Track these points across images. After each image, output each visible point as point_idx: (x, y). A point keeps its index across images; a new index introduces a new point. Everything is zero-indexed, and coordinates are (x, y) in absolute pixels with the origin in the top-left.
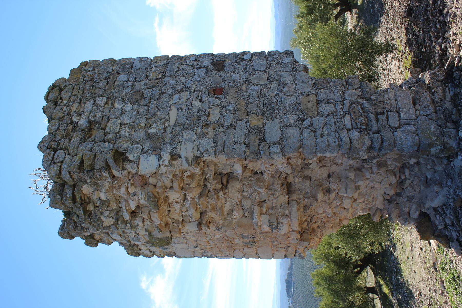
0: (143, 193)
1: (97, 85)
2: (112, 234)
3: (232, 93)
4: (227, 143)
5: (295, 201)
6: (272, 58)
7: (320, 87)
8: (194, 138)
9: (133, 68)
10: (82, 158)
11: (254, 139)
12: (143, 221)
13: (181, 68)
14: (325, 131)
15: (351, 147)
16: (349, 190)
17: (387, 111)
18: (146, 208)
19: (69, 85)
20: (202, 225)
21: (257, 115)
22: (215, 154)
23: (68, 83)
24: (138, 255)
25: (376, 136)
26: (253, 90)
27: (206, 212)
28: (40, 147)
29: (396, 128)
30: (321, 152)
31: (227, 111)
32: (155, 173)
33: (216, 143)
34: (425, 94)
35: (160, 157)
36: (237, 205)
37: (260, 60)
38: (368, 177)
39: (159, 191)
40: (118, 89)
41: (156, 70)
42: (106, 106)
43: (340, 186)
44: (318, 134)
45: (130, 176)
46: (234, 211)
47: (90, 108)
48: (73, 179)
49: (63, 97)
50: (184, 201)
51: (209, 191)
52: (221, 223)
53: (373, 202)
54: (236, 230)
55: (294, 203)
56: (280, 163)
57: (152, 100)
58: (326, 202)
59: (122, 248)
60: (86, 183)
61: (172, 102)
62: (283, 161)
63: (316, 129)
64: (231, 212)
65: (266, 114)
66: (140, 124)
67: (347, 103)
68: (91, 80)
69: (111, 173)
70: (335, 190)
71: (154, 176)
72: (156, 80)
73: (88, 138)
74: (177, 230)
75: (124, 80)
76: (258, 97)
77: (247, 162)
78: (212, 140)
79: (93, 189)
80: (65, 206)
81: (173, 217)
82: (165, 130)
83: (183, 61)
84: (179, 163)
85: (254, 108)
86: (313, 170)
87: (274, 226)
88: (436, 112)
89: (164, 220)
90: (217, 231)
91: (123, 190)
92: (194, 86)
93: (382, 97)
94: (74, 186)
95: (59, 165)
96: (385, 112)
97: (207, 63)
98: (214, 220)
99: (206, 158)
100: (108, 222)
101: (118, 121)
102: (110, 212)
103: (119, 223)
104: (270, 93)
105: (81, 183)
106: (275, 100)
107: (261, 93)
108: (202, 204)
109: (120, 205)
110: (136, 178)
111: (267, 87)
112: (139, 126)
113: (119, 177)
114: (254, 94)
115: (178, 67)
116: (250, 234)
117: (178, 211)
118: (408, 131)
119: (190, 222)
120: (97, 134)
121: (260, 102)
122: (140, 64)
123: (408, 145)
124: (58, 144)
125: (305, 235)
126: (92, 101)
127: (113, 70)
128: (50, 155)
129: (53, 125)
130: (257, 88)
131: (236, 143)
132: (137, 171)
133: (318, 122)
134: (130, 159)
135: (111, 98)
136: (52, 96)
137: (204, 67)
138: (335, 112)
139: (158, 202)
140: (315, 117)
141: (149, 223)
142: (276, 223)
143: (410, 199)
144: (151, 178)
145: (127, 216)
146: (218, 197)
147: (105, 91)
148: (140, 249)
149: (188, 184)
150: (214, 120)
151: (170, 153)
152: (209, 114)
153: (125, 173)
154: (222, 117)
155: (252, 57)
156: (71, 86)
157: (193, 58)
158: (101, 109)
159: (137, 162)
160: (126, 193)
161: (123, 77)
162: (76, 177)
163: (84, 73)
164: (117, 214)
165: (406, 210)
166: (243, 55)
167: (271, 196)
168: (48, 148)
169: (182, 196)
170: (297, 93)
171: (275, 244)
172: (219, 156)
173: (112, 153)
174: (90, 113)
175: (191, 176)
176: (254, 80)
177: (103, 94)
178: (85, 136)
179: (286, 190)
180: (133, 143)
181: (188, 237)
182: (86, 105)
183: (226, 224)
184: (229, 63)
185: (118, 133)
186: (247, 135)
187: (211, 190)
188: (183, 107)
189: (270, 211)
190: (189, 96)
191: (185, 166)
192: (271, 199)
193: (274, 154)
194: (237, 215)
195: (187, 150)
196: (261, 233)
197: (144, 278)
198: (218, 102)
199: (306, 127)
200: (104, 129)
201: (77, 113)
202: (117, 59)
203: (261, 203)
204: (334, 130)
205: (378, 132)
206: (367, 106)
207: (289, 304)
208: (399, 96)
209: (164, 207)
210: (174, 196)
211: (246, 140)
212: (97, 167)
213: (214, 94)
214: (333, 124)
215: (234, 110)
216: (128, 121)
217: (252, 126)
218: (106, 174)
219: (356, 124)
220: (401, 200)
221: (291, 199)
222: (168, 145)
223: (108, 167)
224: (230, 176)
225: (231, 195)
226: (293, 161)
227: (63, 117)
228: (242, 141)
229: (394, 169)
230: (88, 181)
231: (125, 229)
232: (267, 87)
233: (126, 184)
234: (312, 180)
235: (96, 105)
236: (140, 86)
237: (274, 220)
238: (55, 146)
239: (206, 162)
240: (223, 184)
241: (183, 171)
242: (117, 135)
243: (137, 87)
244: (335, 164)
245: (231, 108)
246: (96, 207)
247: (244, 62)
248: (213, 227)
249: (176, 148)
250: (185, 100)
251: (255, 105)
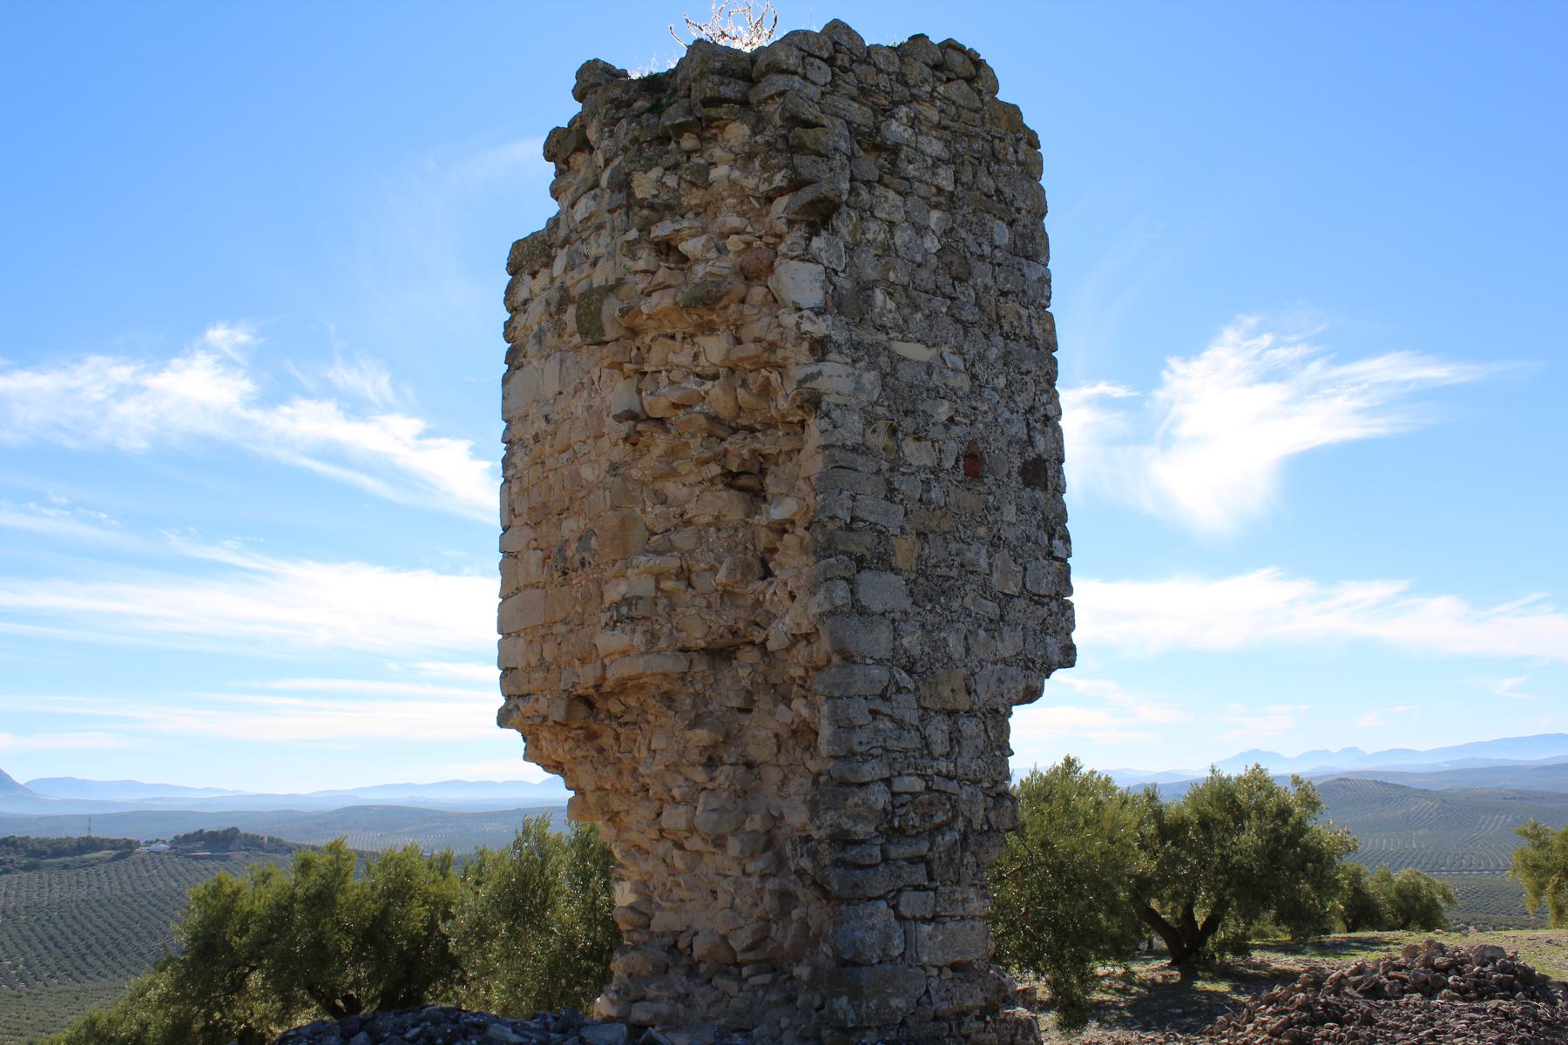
0: (726, 271)
2: (594, 197)
3: (970, 500)
4: (853, 475)
5: (690, 667)
7: (990, 723)
8: (864, 398)
10: (817, 125)
11: (863, 543)
12: (645, 272)
13: (1027, 378)
15: (849, 784)
16: (715, 816)
17: (935, 890)
20: (631, 423)
21: (920, 556)
22: (825, 447)
23: (987, 99)
24: (514, 268)
25: (877, 851)
26: (977, 553)
27: (668, 431)
28: (836, 27)
29: (895, 907)
30: (833, 712)
31: (926, 482)
32: (776, 301)
34: (981, 995)
35: (819, 312)
39: (730, 311)
40: (974, 219)
41: (1020, 317)
42: (934, 190)
43: (725, 795)
44: (878, 704)
45: (772, 240)
46: (663, 508)
47: (929, 151)
48: (765, 101)
49: (954, 86)
50: (698, 375)
51: (723, 440)
52: (634, 472)
55: (681, 665)
59: (540, 225)
60: (754, 133)
62: (805, 622)
65: (921, 580)
66: (894, 269)
67: (952, 787)
68: (993, 155)
69: (781, 191)
73: (859, 142)
74: (619, 359)
78: (859, 439)
79: (737, 149)
80: (695, 80)
81: (656, 348)
82: (882, 328)
83: (1045, 385)
84: (803, 359)
85: (934, 551)
86: (771, 714)
88: (936, 1018)
89: (652, 323)
90: (605, 466)
91: (735, 221)
93: (969, 880)
94: (745, 103)
95: (800, 70)
96: (933, 885)
97: (1041, 443)
98: (642, 456)
99: (815, 426)
100: (645, 185)
101: (898, 217)
102: (675, 190)
104: (971, 595)
105: (753, 120)
106: (955, 605)
109: (690, 215)
111: (985, 590)
112: (888, 268)
113: (768, 213)
114: (969, 556)
115: (1028, 372)
116: (595, 553)
117: (672, 358)
118: (889, 938)
119: (639, 391)
120: (869, 166)
121: (950, 567)
124: (845, 70)
125: (582, 710)
126: (945, 155)
127: (1018, 210)
128: (821, 48)
131: (854, 499)
132: (785, 255)
133: (907, 709)
134: (815, 239)
136: (957, 58)
138: (930, 753)
139: (705, 305)
141: (641, 286)
142: (634, 613)
143: (685, 998)
144: (763, 290)
145: (662, 230)
146: (706, 462)
147: (970, 189)
148: (534, 275)
149: (744, 384)
150: (907, 451)
151: (828, 337)
152: (918, 439)
153: (781, 226)
154: (913, 469)
155: (1057, 559)
158: (927, 177)
159: (807, 257)
160: (725, 230)
161: (1003, 235)
163: (1009, 138)
165: (652, 991)
166: (1061, 538)
167: (704, 603)
168: (835, 44)
169: (712, 371)
170: (973, 663)
171: (561, 629)
172: (820, 458)
173: (832, 195)
174: (916, 149)
175: (766, 391)
178: (862, 134)
179: (720, 643)
180: (850, 249)
181: (585, 394)
182: (934, 142)
187: (725, 445)
188: (935, 376)
189: (663, 602)
190: (960, 393)
192: (697, 601)
194: (653, 514)
195: (835, 377)
196: (599, 584)
197: (242, 338)
198: (948, 464)
200: (880, 181)
201: (916, 117)
203: (684, 575)
204: (888, 745)
205: (886, 859)
206: (947, 838)
207: (149, 843)
208: (973, 928)
209: (684, 324)
210: (715, 349)
212: (797, 159)
215: (930, 502)
216: (898, 242)
217: (894, 540)
218: (779, 179)
219: (903, 805)
221: (695, 656)
222: (846, 334)
223: (796, 185)
224: (757, 496)
225: (708, 496)
226: (802, 651)
229: (773, 940)
230: (758, 138)
232: (985, 590)
233: (749, 229)
234: (740, 716)
236: (982, 275)
237: (641, 610)
238: (839, 62)
239: (799, 429)
240: (739, 474)
243: (980, 268)
244: (785, 776)
245: (935, 494)
246: (689, 154)
248: (620, 452)
249: (840, 353)
251: (943, 554)
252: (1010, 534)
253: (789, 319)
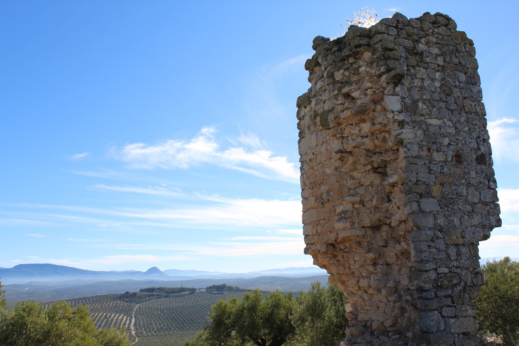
1: (454, 56)
2: (322, 81)
3: (458, 171)
4: (416, 166)
6: (493, 207)
7: (471, 248)
8: (418, 139)
9: (471, 86)
11: (421, 189)
12: (341, 104)
13: (476, 127)
14: (433, 250)
15: (422, 271)
16: (377, 282)
17: (455, 307)
18: (353, 105)
19: (451, 32)
21: (442, 192)
22: (406, 157)
24: (299, 105)
25: (433, 294)
26: (462, 189)
27: (353, 156)
29: (441, 313)
31: (442, 166)
32: (385, 110)
33: (416, 157)
35: (400, 112)
36: (359, 183)
37: (490, 196)
38: (390, 299)
39: (370, 115)
40: (452, 74)
41: (471, 106)
42: (436, 65)
43: (380, 275)
44: (430, 243)
45: (382, 90)
47: (433, 52)
48: (375, 44)
49: (440, 29)
50: (361, 136)
51: (371, 157)
52: (343, 170)
54: (336, 184)
55: (363, 232)
56: (398, 216)
57: (445, 103)
58: (365, 261)
60: (373, 55)
61: (445, 120)
62: (403, 217)
63: (434, 241)
64: (353, 178)
65: (443, 200)
66: (425, 94)
67: (459, 271)
68: (457, 50)
69: (383, 73)
70: (375, 270)
71: (383, 109)
72: (463, 106)
73: (409, 53)
75: (460, 79)
77: (400, 186)
78: (417, 154)
79: (368, 61)
82: (422, 115)
83: (483, 129)
85: (447, 189)
86: (394, 247)
90: (333, 168)
91: (369, 85)
92: (461, 138)
94: (369, 45)
95: (386, 32)
97: (483, 149)
98: (345, 164)
99: (402, 150)
101: (425, 76)
103: (339, 85)
104: (461, 204)
105: (372, 50)
106: (456, 208)
107: (461, 196)
109: (354, 84)
110: (381, 95)
111: (466, 201)
112: (423, 94)
113: (380, 81)
114: (459, 190)
115: (476, 124)
116: (332, 197)
117: (353, 132)
118: (439, 323)
119: (342, 143)
120: (413, 60)
121: (453, 195)
122: (476, 91)
123: (428, 322)
124: (401, 29)
125: (331, 248)
126: (439, 53)
127: (468, 68)
129: (416, 23)
130: (465, 192)
131: (417, 174)
132: (387, 94)
135: (443, 68)
136: (440, 19)
137: (478, 147)
138: (450, 259)
139: (362, 113)
140: (444, 241)
141: (340, 109)
142: (346, 216)
144: (380, 107)
145: (345, 90)
146: (366, 165)
147: (449, 63)
148: (305, 107)
149: (377, 138)
150: (434, 156)
151: (404, 120)
152: (438, 152)
153: (385, 85)
154: (437, 162)
155: (492, 189)
156: (450, 34)
158: (434, 61)
159: (394, 94)
160: (366, 88)
161: (463, 77)
162: (377, 46)
163: (462, 43)
164: (347, 82)
165: (359, 340)
166: (493, 181)
167: (369, 211)
168: (397, 21)
171: (322, 222)
172: (404, 161)
173: (401, 73)
174: (429, 52)
175: (384, 140)
176: (471, 190)
177: (447, 62)
178: (410, 50)
180: (409, 90)
181: (325, 145)
182: (435, 49)
183: (342, 174)
184: (485, 169)
187: (372, 159)
188: (442, 129)
189: (355, 212)
190: (452, 134)
191: (395, 133)
193: (411, 206)
194: (350, 183)
195: (408, 134)
196: (334, 207)
197: (212, 130)
198: (449, 159)
202: (479, 71)
203: (362, 202)
205: (436, 296)
206: (458, 288)
207: (199, 289)
209: (356, 120)
210: (366, 127)
211: (420, 182)
212: (388, 62)
213: (455, 156)
214: (440, 257)
215: (444, 173)
216: (425, 85)
218: (382, 69)
219: (441, 278)
220: (368, 337)
221: (367, 229)
222: (410, 119)
223: (388, 70)
224: (384, 175)
225: (368, 176)
227: (424, 31)
229: (399, 323)
230: (374, 56)
231: (329, 91)
232: (466, 201)
233: (374, 87)
234: (384, 248)
235: (436, 57)
236: (457, 93)
238: (399, 27)
239: (397, 152)
240: (377, 168)
241: (390, 132)
243: (455, 90)
246: (352, 64)
248: (338, 164)
249: (409, 125)
250: (449, 131)
251: (450, 190)
252: (473, 182)
253: (390, 116)
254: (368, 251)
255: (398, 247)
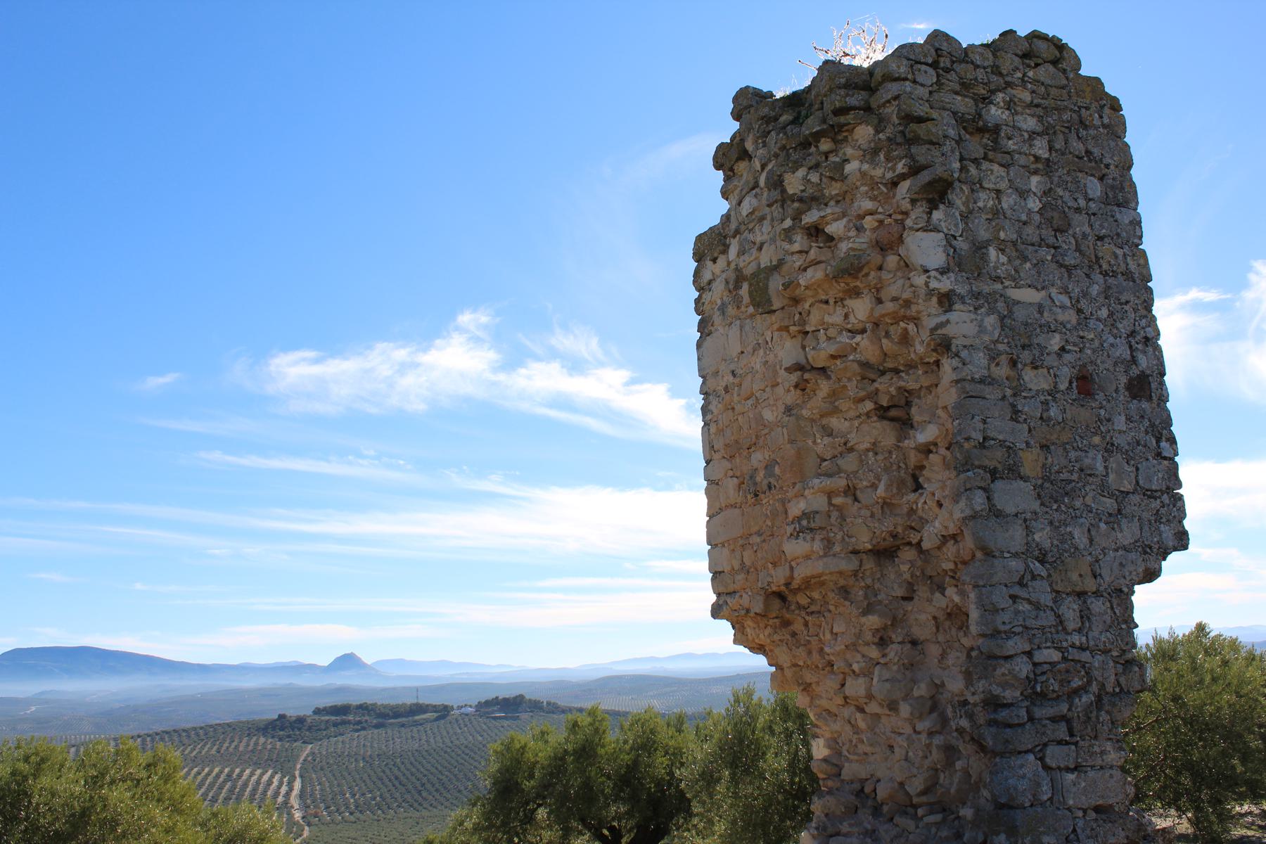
0: (865, 246)
2: (756, 196)
3: (1084, 415)
4: (982, 402)
6: (1167, 501)
7: (1115, 602)
8: (986, 338)
11: (995, 458)
12: (800, 252)
13: (1126, 307)
15: (996, 657)
16: (888, 685)
17: (1076, 744)
19: (1067, 78)
20: (799, 373)
21: (1044, 465)
22: (957, 382)
23: (1071, 76)
24: (699, 256)
25: (1023, 713)
26: (1094, 459)
27: (829, 378)
28: (936, 36)
29: (1042, 759)
30: (980, 597)
31: (1045, 403)
32: (907, 265)
33: (982, 381)
34: (1123, 834)
35: (943, 271)
37: (1160, 475)
38: (920, 726)
39: (870, 278)
40: (1069, 179)
42: (1032, 159)
43: (895, 668)
44: (1017, 590)
45: (900, 217)
47: (1025, 127)
48: (884, 105)
49: (1041, 70)
50: (850, 331)
51: (873, 381)
52: (805, 413)
53: (855, 754)
57: (1053, 251)
58: (859, 635)
60: (877, 132)
64: (828, 432)
65: (1047, 485)
66: (1003, 228)
67: (1085, 657)
69: (903, 177)
72: (1096, 257)
73: (964, 128)
75: (1089, 191)
76: (1082, 470)
77: (943, 451)
78: (985, 373)
79: (865, 147)
82: (997, 279)
83: (1144, 312)
84: (933, 311)
85: (1056, 459)
86: (930, 601)
87: (804, 523)
89: (809, 293)
90: (782, 409)
91: (868, 205)
92: (1092, 336)
94: (868, 109)
95: (910, 76)
96: (1075, 739)
97: (1143, 362)
98: (810, 399)
99: (947, 364)
100: (794, 183)
101: (1003, 185)
104: (1091, 494)
105: (876, 121)
106: (1078, 504)
107: (1090, 475)
108: (846, 368)
109: (832, 203)
110: (896, 229)
111: (1103, 489)
114: (1087, 461)
115: (1127, 302)
116: (778, 478)
117: (827, 319)
118: (1038, 785)
119: (804, 347)
120: (975, 146)
121: (1071, 472)
123: (1010, 781)
124: (947, 70)
125: (777, 603)
126: (1039, 129)
127: (1107, 166)
129: (982, 54)
130: (1100, 467)
131: (984, 422)
134: (935, 212)
136: (1042, 45)
137: (1133, 357)
138: (1064, 629)
140: (1051, 585)
141: (798, 264)
142: (813, 525)
144: (896, 258)
145: (811, 217)
146: (862, 400)
147: (1063, 154)
148: (714, 260)
149: (887, 335)
150: (1026, 378)
151: (953, 291)
152: (1036, 368)
153: (906, 205)
154: (1033, 393)
155: (1165, 458)
156: (1065, 82)
157: (1151, 334)
158: (1025, 149)
159: (929, 228)
160: (861, 212)
161: (1095, 188)
162: (888, 110)
163: (1094, 106)
164: (814, 199)
165: (845, 828)
167: (868, 513)
168: (937, 50)
169: (859, 327)
171: (757, 539)
172: (953, 390)
173: (945, 176)
174: (1014, 127)
175: (905, 339)
176: (1116, 461)
177: (1056, 151)
179: (884, 544)
180: (965, 217)
181: (761, 352)
182: (1029, 118)
183: (802, 423)
184: (1149, 411)
185: (982, 187)
186: (1002, 443)
187: (876, 385)
188: (1046, 314)
189: (835, 514)
190: (1069, 326)
191: (930, 323)
194: (822, 445)
195: (961, 323)
196: (784, 502)
197: (484, 319)
198: (1063, 387)
199: (1028, 566)
200: (985, 158)
201: (1011, 100)
203: (851, 492)
204: (1027, 624)
205: (1031, 719)
208: (1111, 776)
209: (835, 290)
210: (861, 308)
212: (914, 150)
215: (1050, 419)
216: (1005, 206)
218: (901, 167)
219: (1043, 673)
220: (867, 820)
222: (967, 287)
223: (915, 170)
224: (905, 424)
225: (865, 427)
227: (1001, 74)
228: (991, 434)
230: (881, 136)
231: (772, 220)
232: (1103, 489)
233: (880, 210)
235: (1031, 138)
236: (1080, 225)
238: (942, 65)
239: (935, 368)
240: (888, 408)
241: (918, 319)
242: (977, 186)
243: (1077, 218)
246: (826, 155)
247: (1154, 442)
248: (792, 397)
249: (963, 303)
250: (1061, 318)
251: (1064, 462)
252: (1120, 440)
253: (919, 280)
254: (867, 611)
255: (940, 601)
